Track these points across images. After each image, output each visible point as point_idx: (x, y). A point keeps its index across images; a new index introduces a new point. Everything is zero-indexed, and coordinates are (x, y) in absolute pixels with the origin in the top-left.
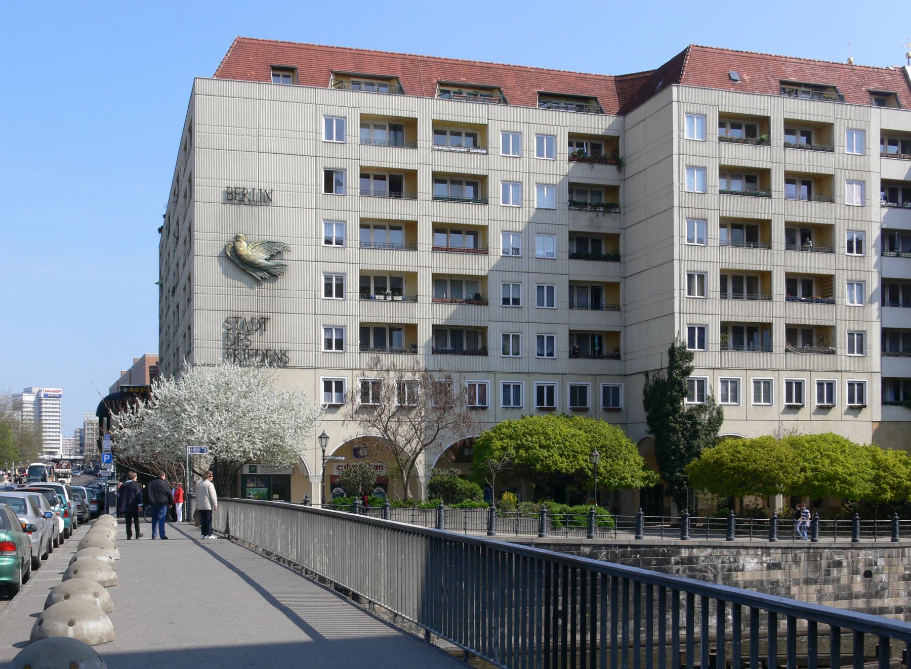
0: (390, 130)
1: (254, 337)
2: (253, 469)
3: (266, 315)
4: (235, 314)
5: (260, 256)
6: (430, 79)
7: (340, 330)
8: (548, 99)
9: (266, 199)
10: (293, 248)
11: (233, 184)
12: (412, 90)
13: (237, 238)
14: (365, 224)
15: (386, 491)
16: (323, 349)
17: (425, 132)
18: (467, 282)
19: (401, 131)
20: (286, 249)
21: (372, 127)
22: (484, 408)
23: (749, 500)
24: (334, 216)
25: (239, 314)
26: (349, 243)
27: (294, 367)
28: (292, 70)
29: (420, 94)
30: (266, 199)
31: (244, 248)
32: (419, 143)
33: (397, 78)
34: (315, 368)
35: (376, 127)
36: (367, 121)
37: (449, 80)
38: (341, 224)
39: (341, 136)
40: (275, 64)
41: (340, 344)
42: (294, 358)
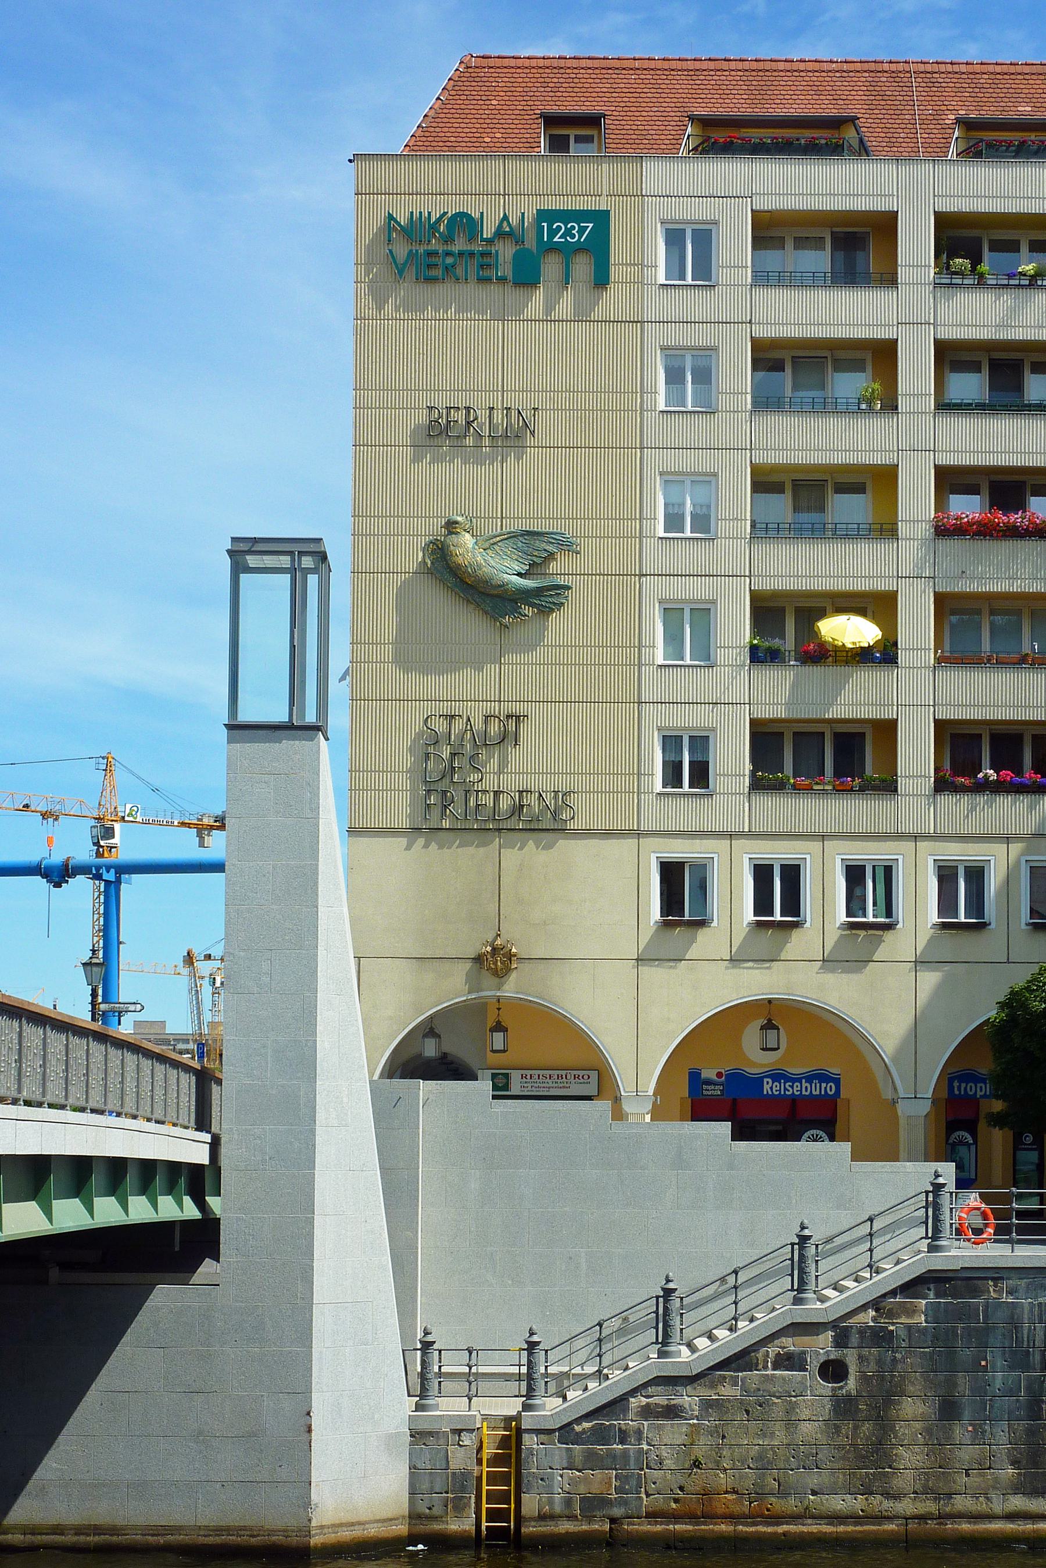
0: (834, 248)
2: (501, 1082)
3: (518, 708)
4: (445, 708)
5: (505, 569)
6: (938, 115)
7: (701, 742)
8: (723, 136)
10: (586, 546)
11: (441, 401)
12: (891, 144)
13: (451, 526)
15: (975, 1142)
16: (658, 787)
17: (916, 246)
18: (1033, 613)
19: (859, 246)
20: (567, 546)
21: (789, 244)
22: (982, 926)
23: (1029, 1139)
24: (688, 461)
25: (456, 708)
26: (723, 528)
27: (588, 833)
28: (593, 121)
29: (903, 153)
31: (467, 548)
32: (902, 274)
33: (853, 120)
34: (638, 834)
35: (801, 243)
36: (770, 230)
37: (989, 112)
38: (708, 479)
39: (704, 269)
40: (553, 109)
41: (701, 775)
42: (585, 813)
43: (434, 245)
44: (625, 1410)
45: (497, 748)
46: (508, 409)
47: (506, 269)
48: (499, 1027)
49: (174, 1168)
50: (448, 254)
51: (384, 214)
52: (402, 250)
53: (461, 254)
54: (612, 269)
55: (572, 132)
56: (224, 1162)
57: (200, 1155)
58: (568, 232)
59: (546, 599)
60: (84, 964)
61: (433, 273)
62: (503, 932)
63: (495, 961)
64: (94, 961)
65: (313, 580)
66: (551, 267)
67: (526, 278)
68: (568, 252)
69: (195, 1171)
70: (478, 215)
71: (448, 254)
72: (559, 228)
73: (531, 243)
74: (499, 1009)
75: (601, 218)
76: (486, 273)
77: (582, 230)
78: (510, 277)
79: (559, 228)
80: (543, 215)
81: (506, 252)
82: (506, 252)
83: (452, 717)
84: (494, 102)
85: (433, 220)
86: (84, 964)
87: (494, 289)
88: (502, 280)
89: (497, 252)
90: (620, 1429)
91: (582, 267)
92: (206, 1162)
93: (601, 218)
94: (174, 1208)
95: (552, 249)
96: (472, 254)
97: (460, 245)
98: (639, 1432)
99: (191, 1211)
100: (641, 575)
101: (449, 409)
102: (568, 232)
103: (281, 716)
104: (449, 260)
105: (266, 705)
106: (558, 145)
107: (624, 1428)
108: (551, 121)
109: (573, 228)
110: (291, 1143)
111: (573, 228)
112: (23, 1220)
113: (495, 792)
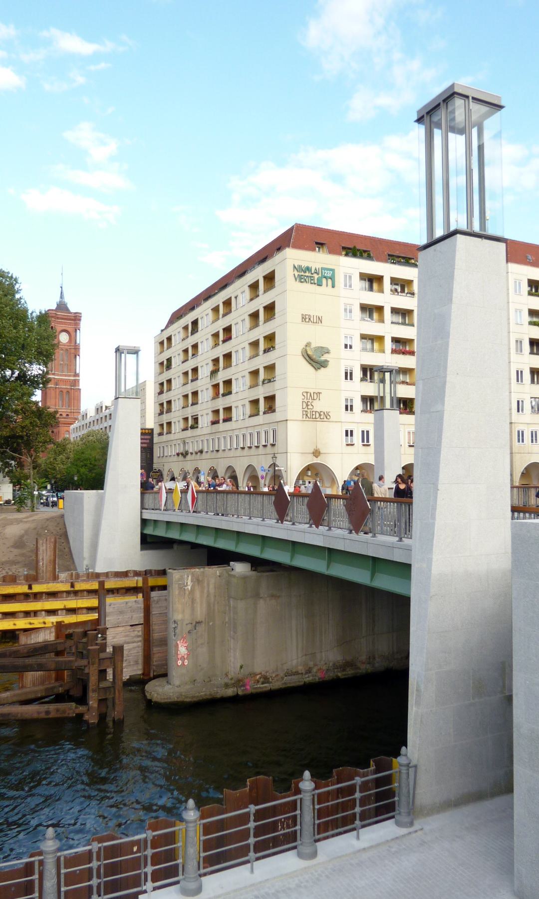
1: (315, 403)
14: (364, 337)
30: (320, 320)
52: (296, 274)
63: (316, 453)
66: (324, 281)
75: (333, 270)
81: (316, 276)
93: (333, 270)
97: (307, 274)
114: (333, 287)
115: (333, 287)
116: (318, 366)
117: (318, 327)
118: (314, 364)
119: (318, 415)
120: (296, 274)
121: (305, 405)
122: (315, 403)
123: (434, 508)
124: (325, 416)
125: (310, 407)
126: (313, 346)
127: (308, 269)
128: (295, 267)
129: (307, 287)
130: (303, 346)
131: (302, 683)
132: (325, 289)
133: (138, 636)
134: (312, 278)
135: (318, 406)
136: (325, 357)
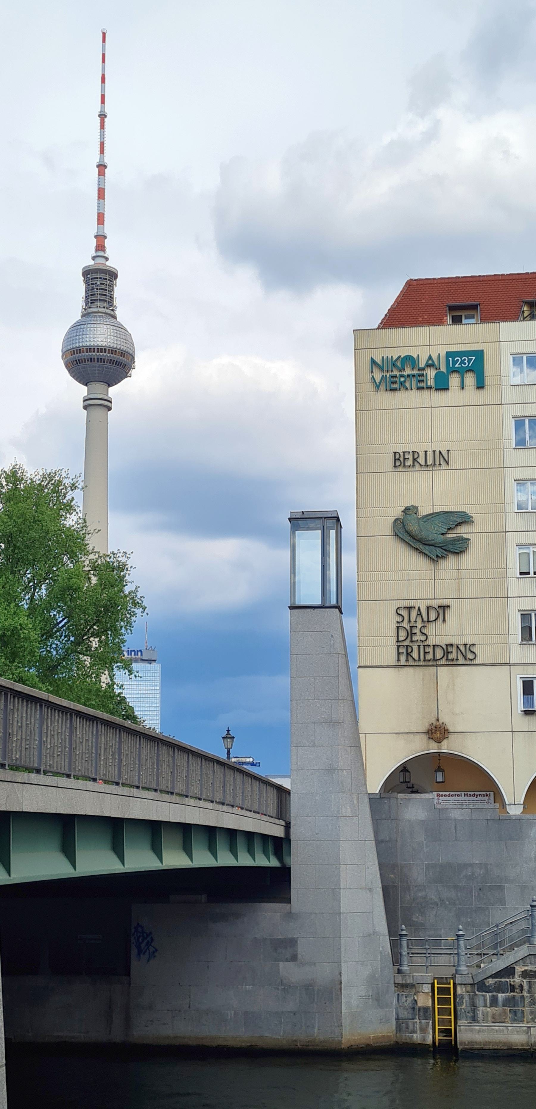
1: (431, 630)
3: (445, 602)
4: (406, 604)
9: (441, 459)
10: (476, 518)
25: (412, 603)
30: (441, 459)
43: (396, 373)
44: (513, 974)
45: (434, 623)
46: (434, 451)
47: (431, 382)
48: (439, 769)
49: (265, 838)
50: (402, 376)
51: (369, 358)
52: (378, 376)
53: (408, 376)
54: (486, 378)
55: (463, 314)
56: (293, 837)
57: (278, 832)
58: (463, 362)
59: (458, 548)
60: (223, 738)
61: (394, 386)
62: (440, 718)
63: (437, 732)
64: (229, 736)
65: (333, 533)
66: (454, 380)
67: (442, 386)
68: (461, 372)
69: (276, 839)
70: (416, 356)
71: (402, 376)
72: (458, 360)
73: (443, 369)
74: (439, 760)
75: (479, 354)
76: (421, 385)
77: (469, 361)
78: (433, 385)
79: (458, 360)
80: (449, 354)
81: (431, 374)
82: (431, 374)
83: (411, 607)
84: (423, 301)
85: (394, 359)
86: (223, 738)
87: (426, 393)
88: (430, 388)
89: (426, 374)
90: (510, 984)
91: (470, 379)
92: (282, 835)
93: (479, 354)
94: (263, 860)
95: (456, 371)
96: (414, 376)
97: (408, 371)
98: (521, 986)
99: (274, 863)
100: (506, 532)
101: (404, 452)
102: (463, 362)
103: (319, 602)
104: (402, 379)
105: (310, 593)
106: (457, 320)
107: (512, 983)
108: (452, 308)
109: (465, 359)
110: (327, 825)
111: (465, 359)
112: (36, 864)
113: (434, 646)
114: (480, 386)
115: (480, 386)
116: (439, 552)
117: (441, 476)
118: (426, 549)
119: (439, 654)
120: (378, 376)
121: (403, 635)
122: (431, 630)
123: (130, 966)
124: (459, 655)
125: (418, 637)
126: (424, 511)
127: (409, 360)
128: (373, 362)
129: (411, 398)
130: (397, 512)
131: (178, 1044)
132: (460, 394)
133: (25, 762)
134: (421, 378)
135: (439, 634)
136: (463, 531)
